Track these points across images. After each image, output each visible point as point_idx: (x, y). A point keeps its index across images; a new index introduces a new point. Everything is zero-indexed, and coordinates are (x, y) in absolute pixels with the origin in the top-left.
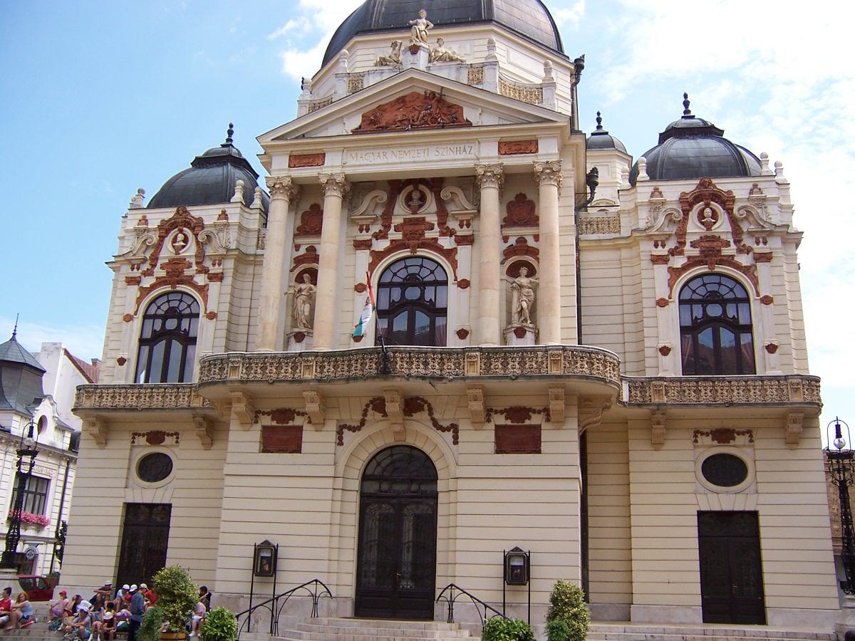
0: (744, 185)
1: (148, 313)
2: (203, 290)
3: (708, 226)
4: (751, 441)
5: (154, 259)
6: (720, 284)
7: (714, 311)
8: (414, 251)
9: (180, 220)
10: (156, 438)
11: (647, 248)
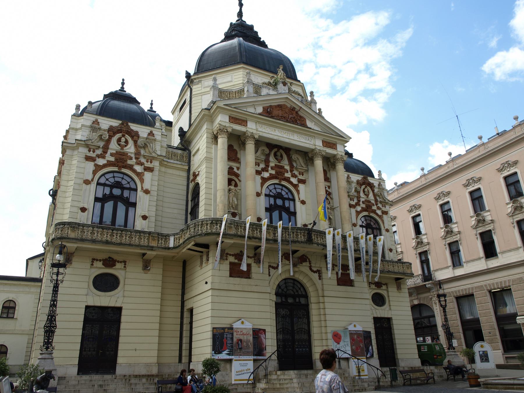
0: (89, 118)
1: (99, 182)
2: (140, 175)
3: (122, 147)
4: (125, 267)
5: (106, 148)
6: (123, 178)
7: (117, 192)
8: (280, 181)
9: (124, 129)
10: (110, 262)
11: (83, 151)
